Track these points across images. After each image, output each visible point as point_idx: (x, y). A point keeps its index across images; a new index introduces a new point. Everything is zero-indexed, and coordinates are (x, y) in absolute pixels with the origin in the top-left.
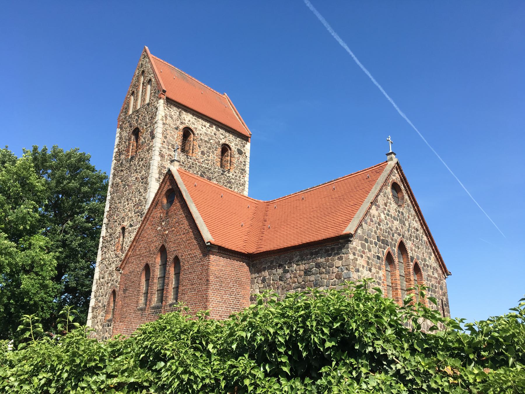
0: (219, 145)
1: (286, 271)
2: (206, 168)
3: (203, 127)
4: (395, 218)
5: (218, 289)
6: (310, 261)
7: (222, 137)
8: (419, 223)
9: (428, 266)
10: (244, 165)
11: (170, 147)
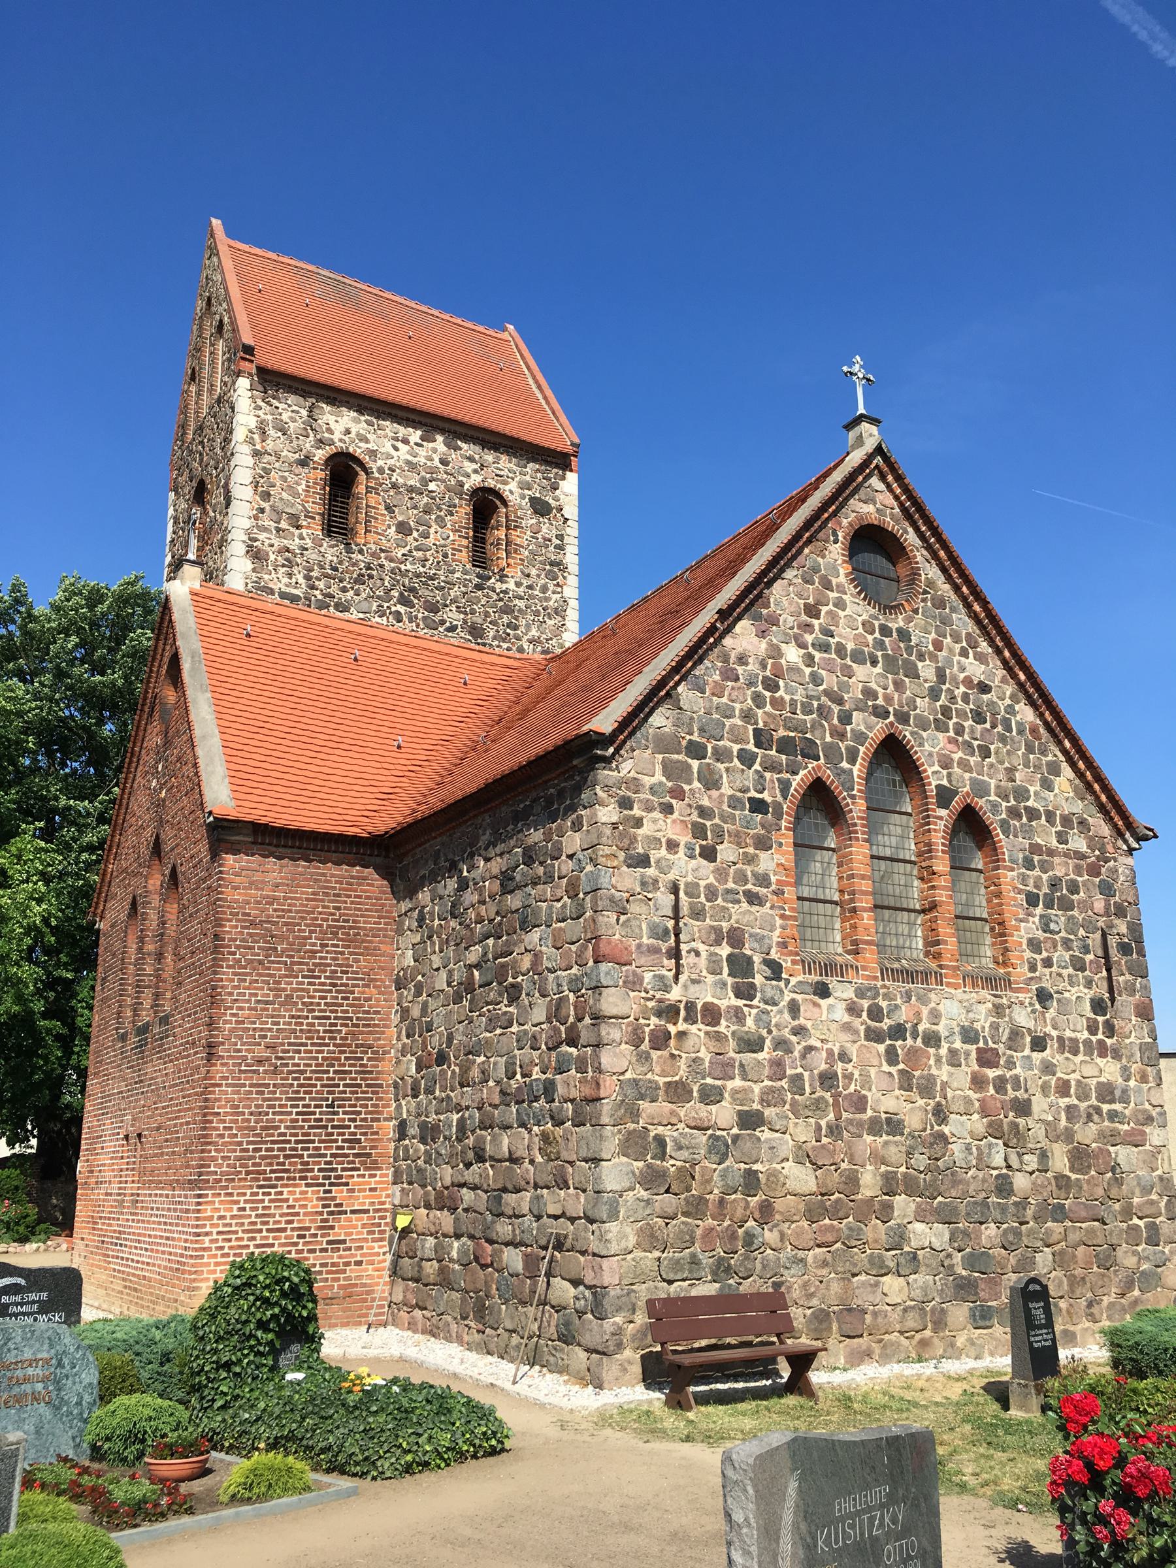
0: (460, 494)
1: (463, 885)
2: (418, 576)
3: (399, 445)
4: (858, 657)
5: (260, 962)
6: (512, 842)
7: (469, 467)
8: (995, 662)
9: (1033, 814)
10: (560, 548)
11: (284, 525)
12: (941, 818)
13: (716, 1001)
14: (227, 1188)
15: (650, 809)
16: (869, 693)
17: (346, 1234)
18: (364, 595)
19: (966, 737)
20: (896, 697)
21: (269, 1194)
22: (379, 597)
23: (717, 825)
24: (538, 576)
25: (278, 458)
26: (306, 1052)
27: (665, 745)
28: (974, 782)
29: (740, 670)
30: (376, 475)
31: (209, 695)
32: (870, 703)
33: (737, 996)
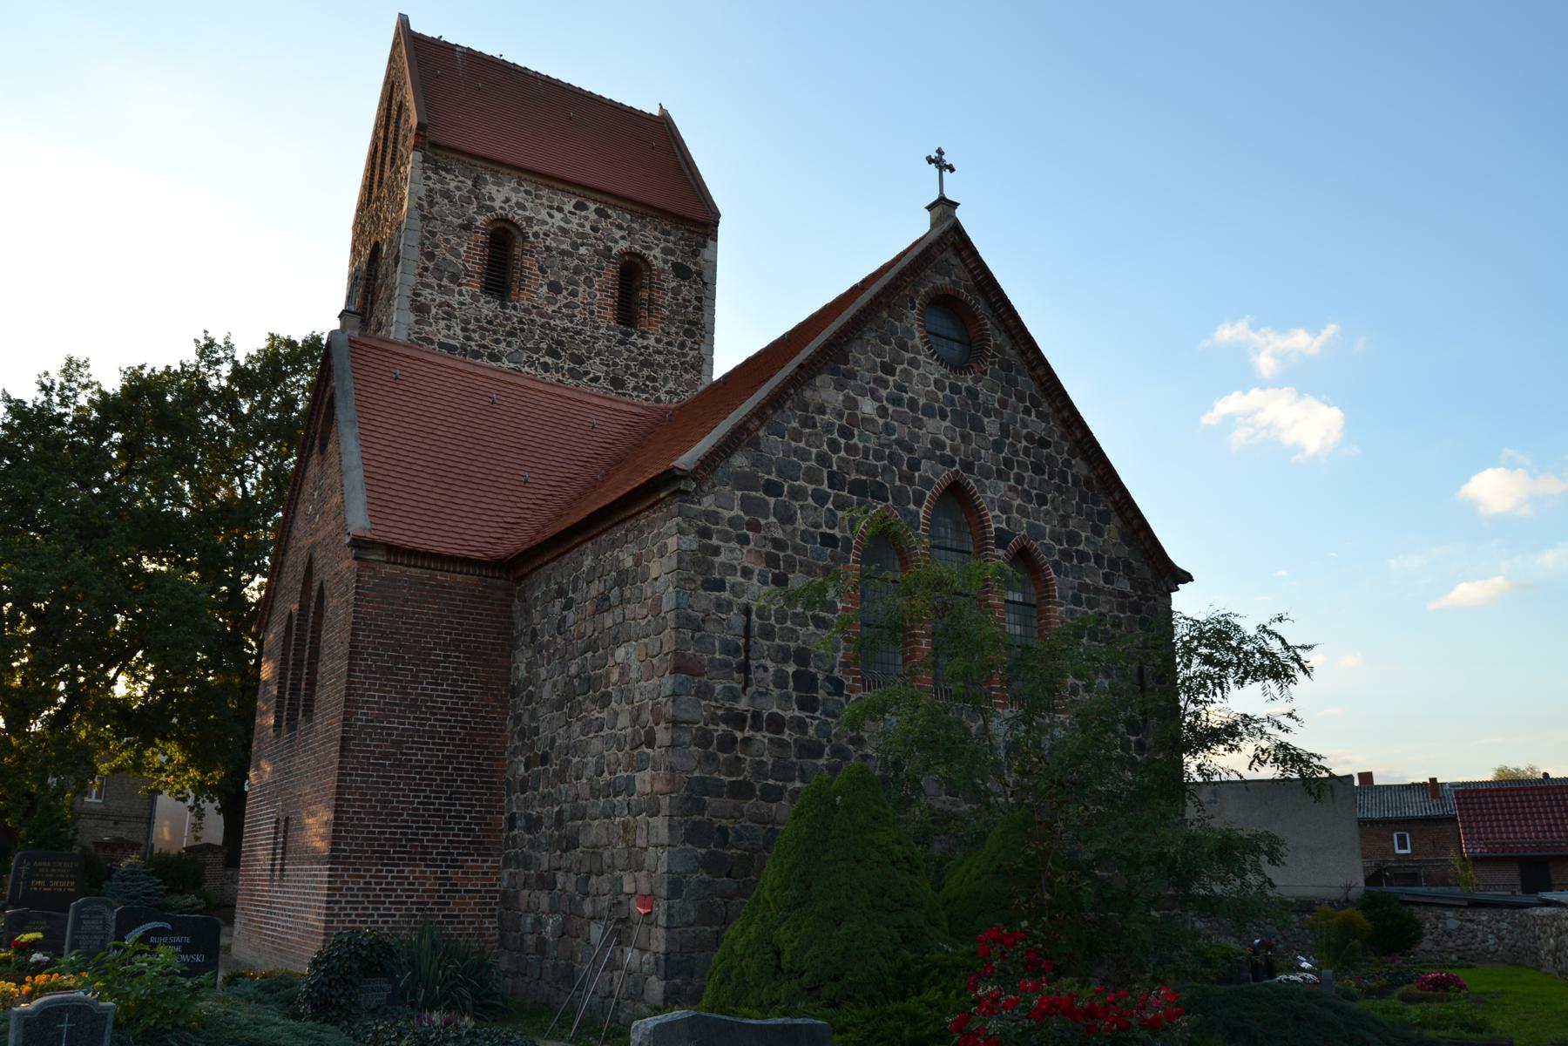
2: (565, 330)
3: (555, 213)
4: (929, 411)
7: (618, 234)
9: (1083, 557)
11: (445, 282)
15: (728, 540)
28: (1030, 526)
29: (818, 417)
33: (800, 709)
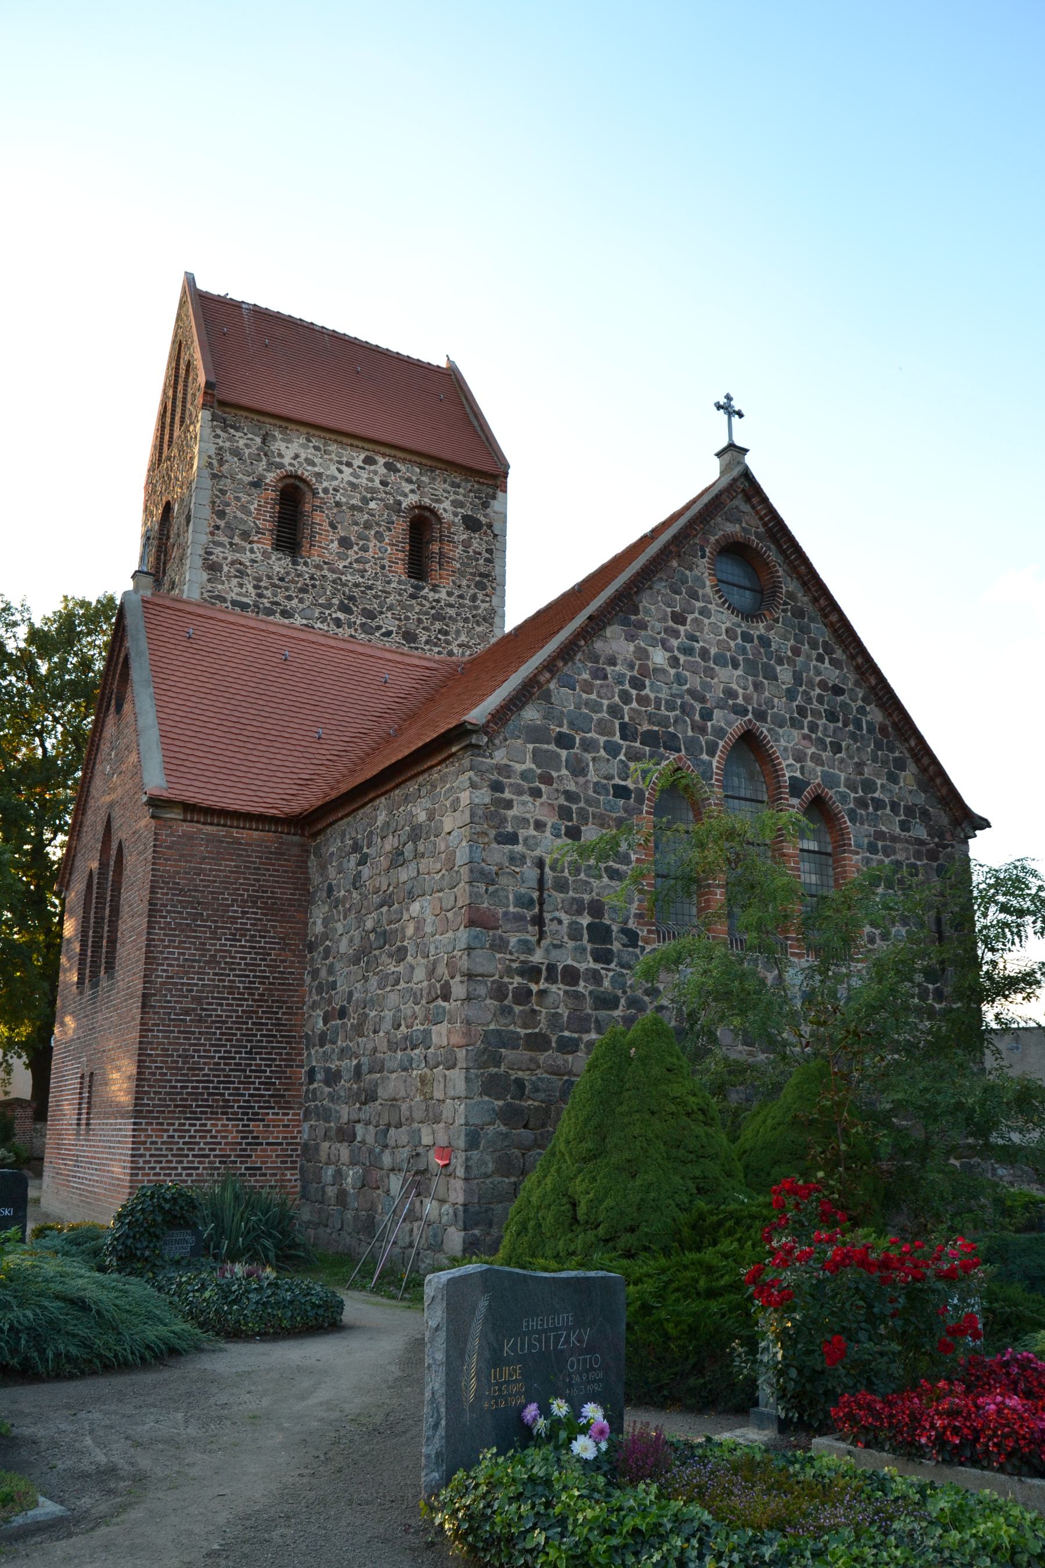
3: (344, 468)
4: (721, 660)
7: (407, 487)
9: (878, 804)
12: (793, 806)
13: (575, 964)
14: (158, 1118)
15: (520, 793)
16: (730, 694)
17: (262, 1162)
18: (307, 603)
19: (820, 734)
20: (755, 697)
21: (195, 1125)
22: (321, 605)
23: (582, 809)
24: (469, 586)
25: (233, 479)
26: (228, 1005)
27: (536, 734)
29: (609, 669)
30: (322, 495)
31: (152, 690)
32: (731, 702)
33: (596, 960)
